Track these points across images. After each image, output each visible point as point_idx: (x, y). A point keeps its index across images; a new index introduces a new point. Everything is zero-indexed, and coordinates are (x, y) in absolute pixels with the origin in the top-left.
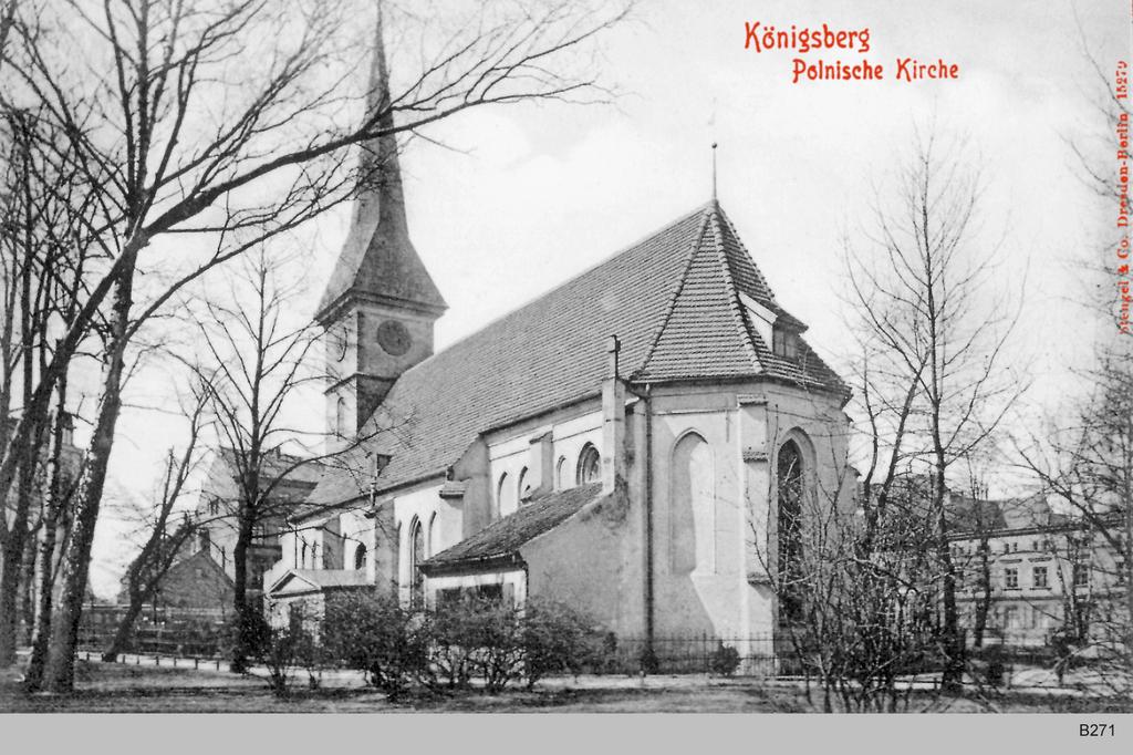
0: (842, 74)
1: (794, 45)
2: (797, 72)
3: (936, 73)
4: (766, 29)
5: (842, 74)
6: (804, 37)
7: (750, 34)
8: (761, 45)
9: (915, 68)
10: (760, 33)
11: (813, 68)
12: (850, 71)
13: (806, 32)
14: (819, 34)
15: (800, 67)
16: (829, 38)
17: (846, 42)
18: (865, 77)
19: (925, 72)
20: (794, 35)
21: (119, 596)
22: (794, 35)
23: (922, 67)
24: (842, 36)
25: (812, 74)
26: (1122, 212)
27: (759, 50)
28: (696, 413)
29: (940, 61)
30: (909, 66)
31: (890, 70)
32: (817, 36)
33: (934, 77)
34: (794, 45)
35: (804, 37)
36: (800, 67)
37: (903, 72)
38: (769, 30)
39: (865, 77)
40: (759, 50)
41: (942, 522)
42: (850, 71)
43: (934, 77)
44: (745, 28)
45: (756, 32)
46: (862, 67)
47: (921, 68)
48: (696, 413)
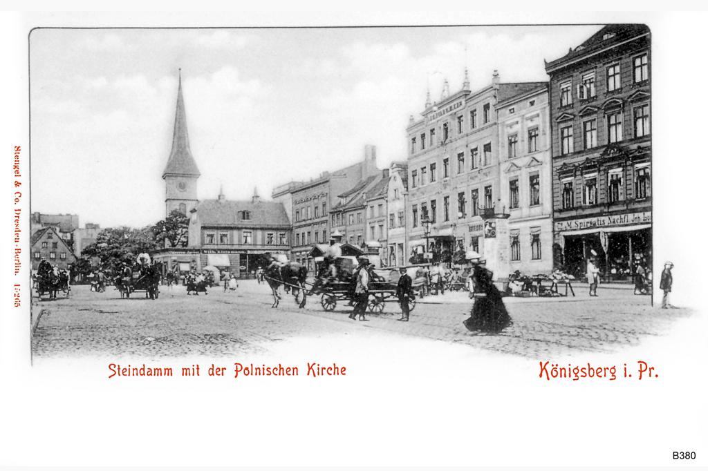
0: (266, 372)
1: (570, 376)
2: (237, 371)
3: (332, 372)
4: (553, 365)
5: (266, 372)
6: (576, 371)
7: (543, 369)
8: (550, 376)
9: (318, 368)
10: (549, 368)
11: (247, 369)
12: (271, 370)
13: (577, 368)
14: (585, 369)
15: (239, 368)
16: (591, 371)
17: (602, 374)
18: (334, 374)
19: (325, 371)
20: (570, 369)
21: (136, 230)
22: (570, 369)
23: (323, 368)
24: (599, 370)
25: (246, 372)
26: (18, 217)
27: (548, 379)
28: (531, 220)
29: (280, 365)
30: (315, 368)
31: (303, 369)
32: (584, 370)
33: (330, 374)
34: (570, 376)
35: (576, 371)
36: (239, 368)
37: (311, 371)
38: (555, 366)
39: (334, 374)
40: (548, 379)
41: (459, 269)
42: (271, 370)
43: (330, 374)
44: (539, 365)
45: (547, 367)
46: (333, 368)
47: (323, 369)
48: (531, 220)
